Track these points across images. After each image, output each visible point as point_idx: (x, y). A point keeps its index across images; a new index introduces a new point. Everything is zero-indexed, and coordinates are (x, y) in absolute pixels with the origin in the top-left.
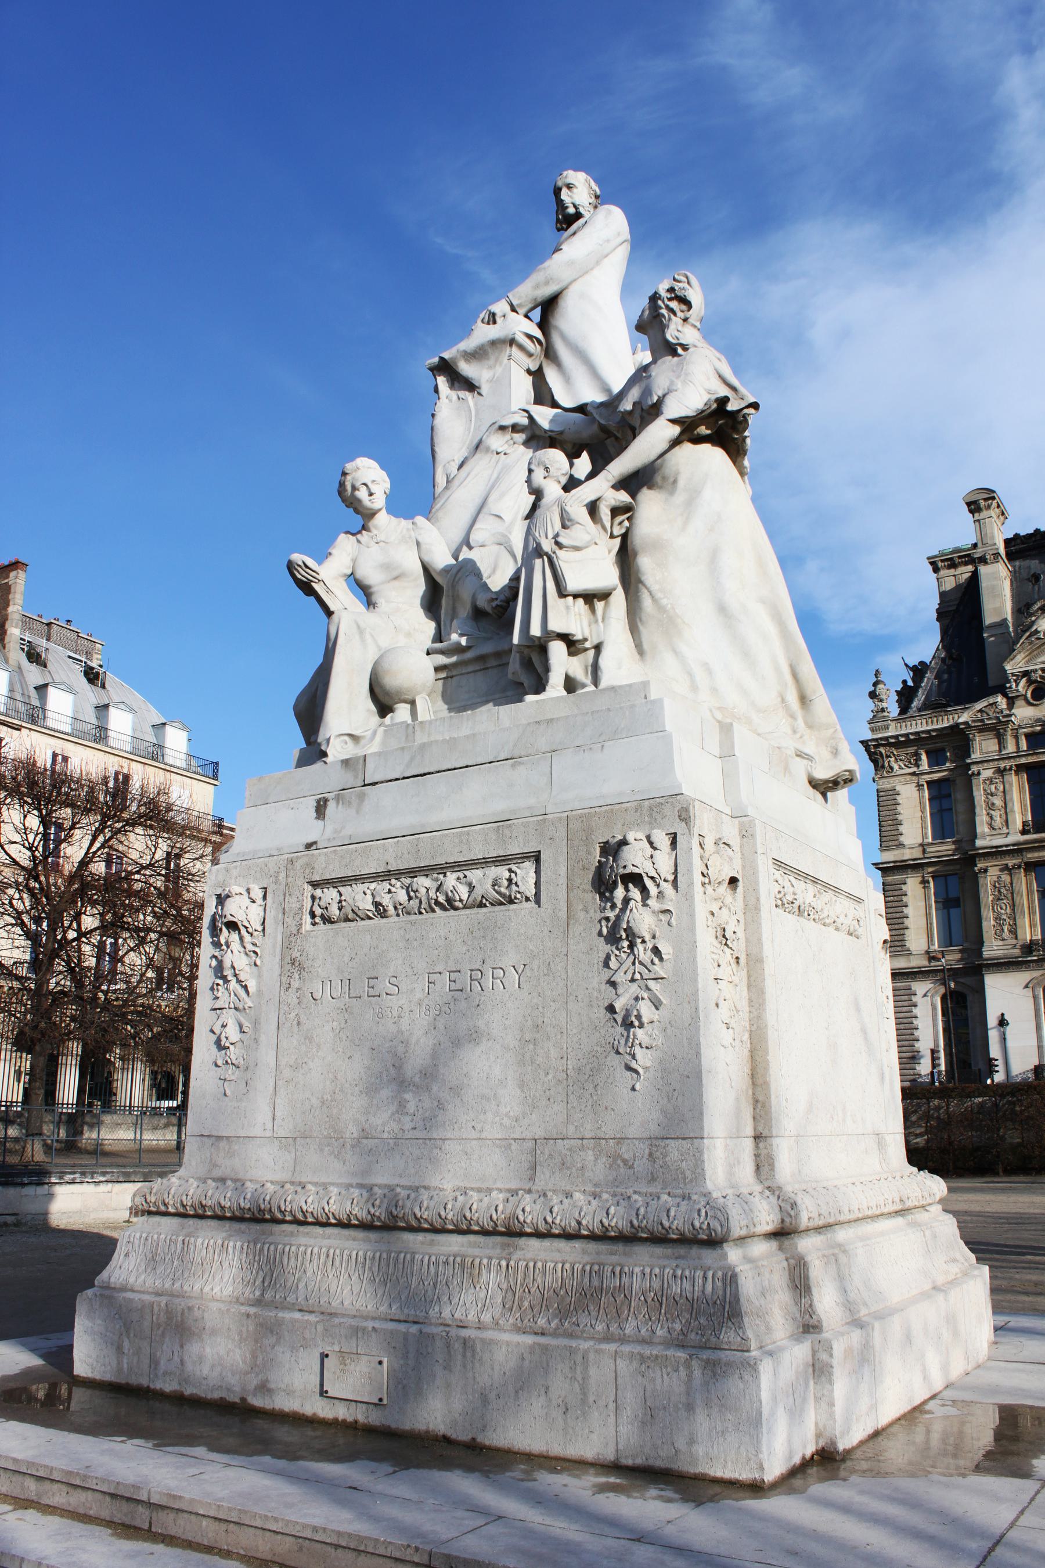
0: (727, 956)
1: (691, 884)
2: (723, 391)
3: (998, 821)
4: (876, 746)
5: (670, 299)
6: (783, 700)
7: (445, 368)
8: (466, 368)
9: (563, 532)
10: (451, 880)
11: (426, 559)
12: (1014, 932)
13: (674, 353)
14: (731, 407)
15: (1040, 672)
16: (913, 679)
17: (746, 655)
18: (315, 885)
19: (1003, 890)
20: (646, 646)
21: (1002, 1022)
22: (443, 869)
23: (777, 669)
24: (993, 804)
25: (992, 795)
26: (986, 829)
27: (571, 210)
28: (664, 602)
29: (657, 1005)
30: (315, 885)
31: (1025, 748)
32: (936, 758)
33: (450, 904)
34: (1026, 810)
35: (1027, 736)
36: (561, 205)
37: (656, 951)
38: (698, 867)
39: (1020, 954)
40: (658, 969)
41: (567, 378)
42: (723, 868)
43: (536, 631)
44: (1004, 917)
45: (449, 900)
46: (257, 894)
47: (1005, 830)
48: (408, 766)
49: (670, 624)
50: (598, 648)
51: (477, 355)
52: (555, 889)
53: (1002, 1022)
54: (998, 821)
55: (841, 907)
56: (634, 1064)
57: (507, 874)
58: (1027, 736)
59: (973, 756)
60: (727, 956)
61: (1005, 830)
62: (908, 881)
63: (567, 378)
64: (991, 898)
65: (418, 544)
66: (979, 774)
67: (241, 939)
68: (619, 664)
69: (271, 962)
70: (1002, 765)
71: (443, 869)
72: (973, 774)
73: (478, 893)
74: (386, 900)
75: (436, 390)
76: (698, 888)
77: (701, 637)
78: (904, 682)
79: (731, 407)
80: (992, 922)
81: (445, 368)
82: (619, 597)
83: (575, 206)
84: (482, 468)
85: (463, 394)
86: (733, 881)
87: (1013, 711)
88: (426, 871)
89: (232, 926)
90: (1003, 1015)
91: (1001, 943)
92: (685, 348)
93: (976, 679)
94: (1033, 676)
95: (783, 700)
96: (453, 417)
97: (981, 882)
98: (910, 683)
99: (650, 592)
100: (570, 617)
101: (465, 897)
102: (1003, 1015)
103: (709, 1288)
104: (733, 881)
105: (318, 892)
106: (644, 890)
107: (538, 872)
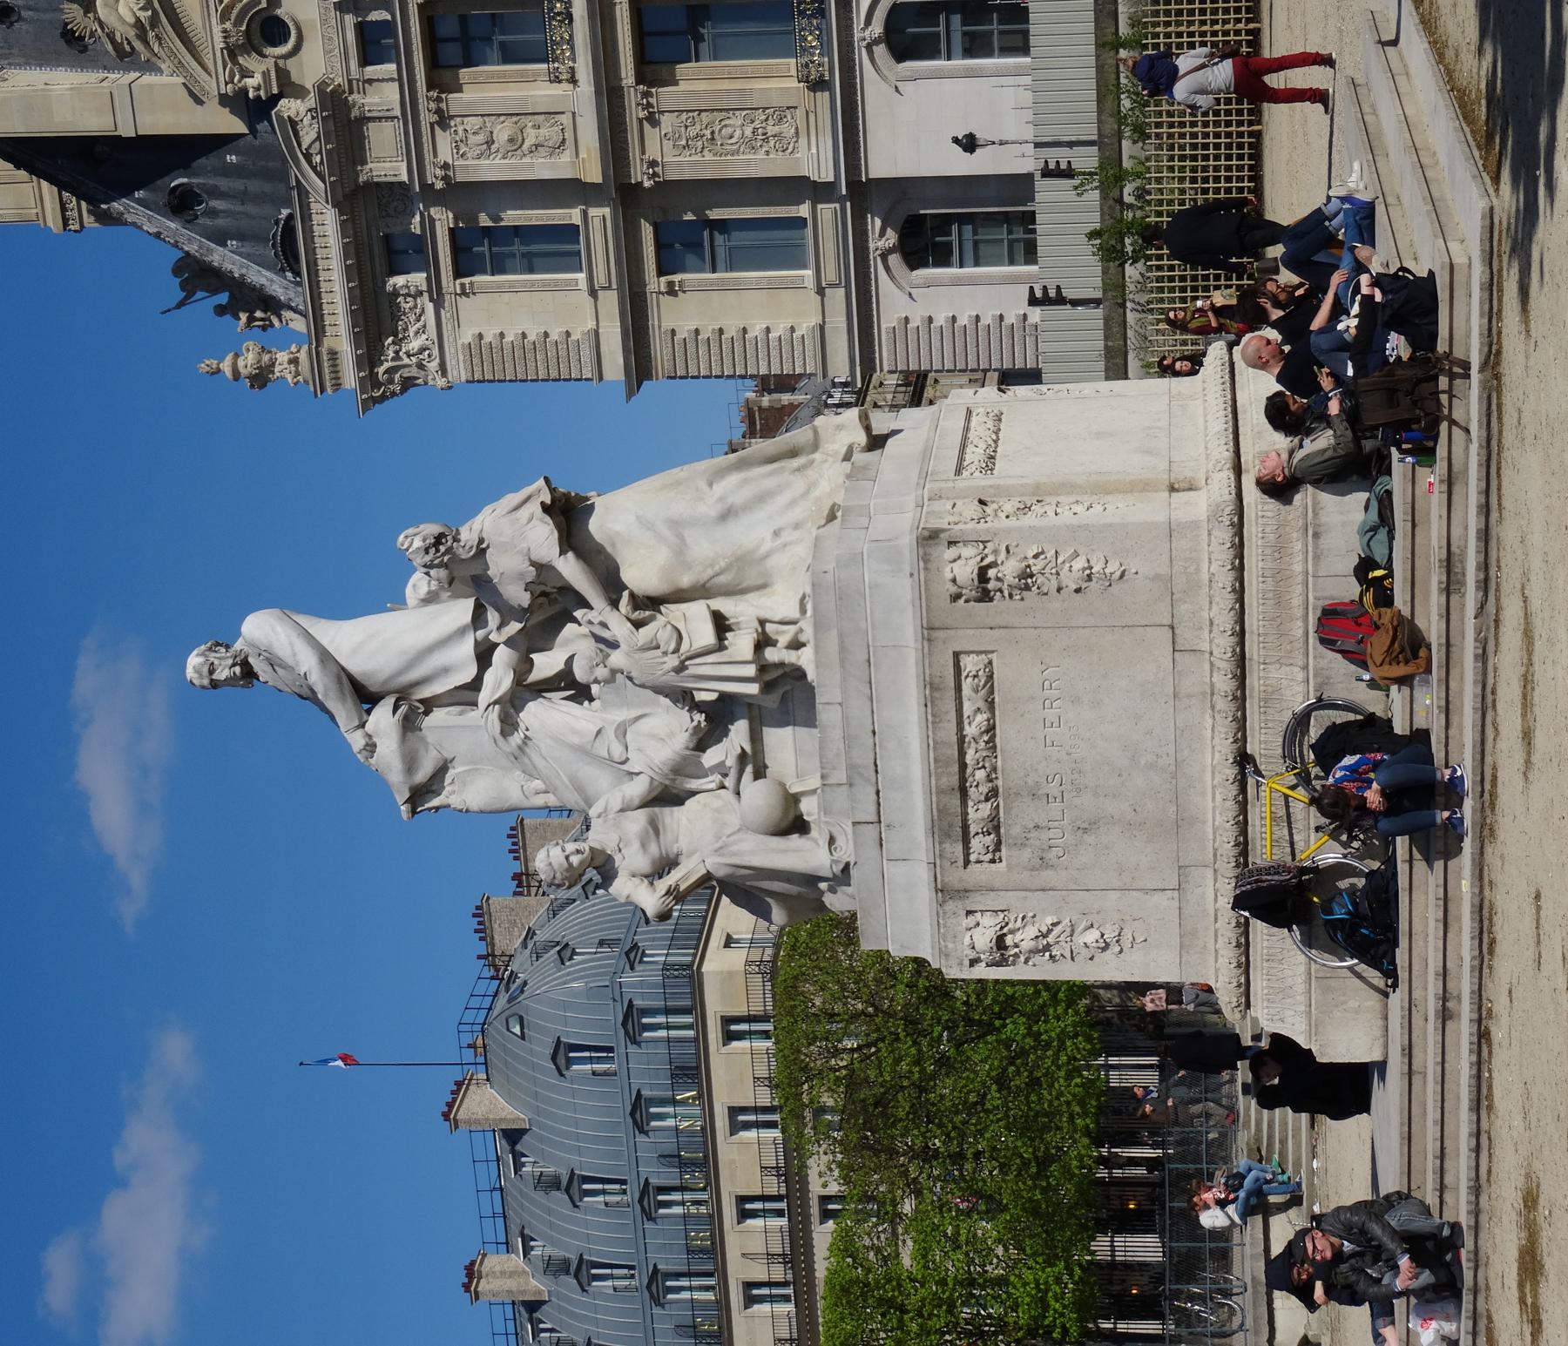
0: (1036, 508)
1: (988, 530)
2: (534, 507)
3: (548, 133)
4: (377, 384)
5: (437, 551)
6: (798, 470)
7: (418, 795)
8: (422, 775)
9: (663, 648)
10: (970, 730)
11: (637, 802)
12: (782, 113)
13: (484, 551)
14: (548, 501)
15: (228, 25)
16: (214, 291)
17: (762, 498)
18: (967, 862)
19: (692, 132)
20: (760, 582)
21: (969, 144)
22: (961, 739)
23: (770, 474)
24: (511, 140)
25: (490, 142)
26: (567, 157)
27: (237, 669)
28: (723, 564)
29: (1076, 555)
30: (967, 862)
31: (393, 67)
32: (404, 252)
33: (991, 729)
34: (522, 73)
35: (365, 61)
36: (230, 681)
37: (1036, 556)
38: (972, 525)
39: (827, 94)
40: (1050, 554)
41: (445, 671)
42: (973, 509)
43: (751, 670)
44: (748, 131)
45: (987, 732)
46: (971, 920)
47: (566, 119)
48: (868, 780)
49: (743, 560)
50: (762, 622)
51: (410, 764)
52: (986, 640)
53: (969, 144)
54: (548, 133)
55: (980, 429)
56: (1118, 574)
57: (969, 680)
58: (365, 61)
59: (405, 178)
60: (1036, 508)
61: (566, 119)
62: (667, 324)
63: (445, 671)
64: (708, 156)
65: (622, 810)
66: (446, 166)
67: (1012, 932)
68: (779, 603)
69: (1035, 901)
70: (427, 118)
71: (961, 739)
72: (445, 178)
73: (981, 704)
74: (984, 789)
75: (437, 809)
76: (989, 525)
77: (752, 533)
78: (220, 310)
79: (548, 501)
80: (761, 155)
81: (418, 795)
82: (719, 604)
83: (234, 665)
84: (545, 753)
85: (448, 780)
86: (982, 502)
87: (309, 86)
88: (962, 753)
89: (1000, 942)
90: (956, 140)
91: (803, 141)
92: (481, 541)
93: (232, 158)
94: (237, 38)
95: (798, 470)
96: (473, 790)
97: (673, 175)
98: (223, 298)
99: (718, 574)
100: (741, 644)
101: (985, 716)
102: (956, 140)
103: (1270, 514)
104: (982, 502)
105: (973, 858)
106: (989, 566)
107: (969, 653)
